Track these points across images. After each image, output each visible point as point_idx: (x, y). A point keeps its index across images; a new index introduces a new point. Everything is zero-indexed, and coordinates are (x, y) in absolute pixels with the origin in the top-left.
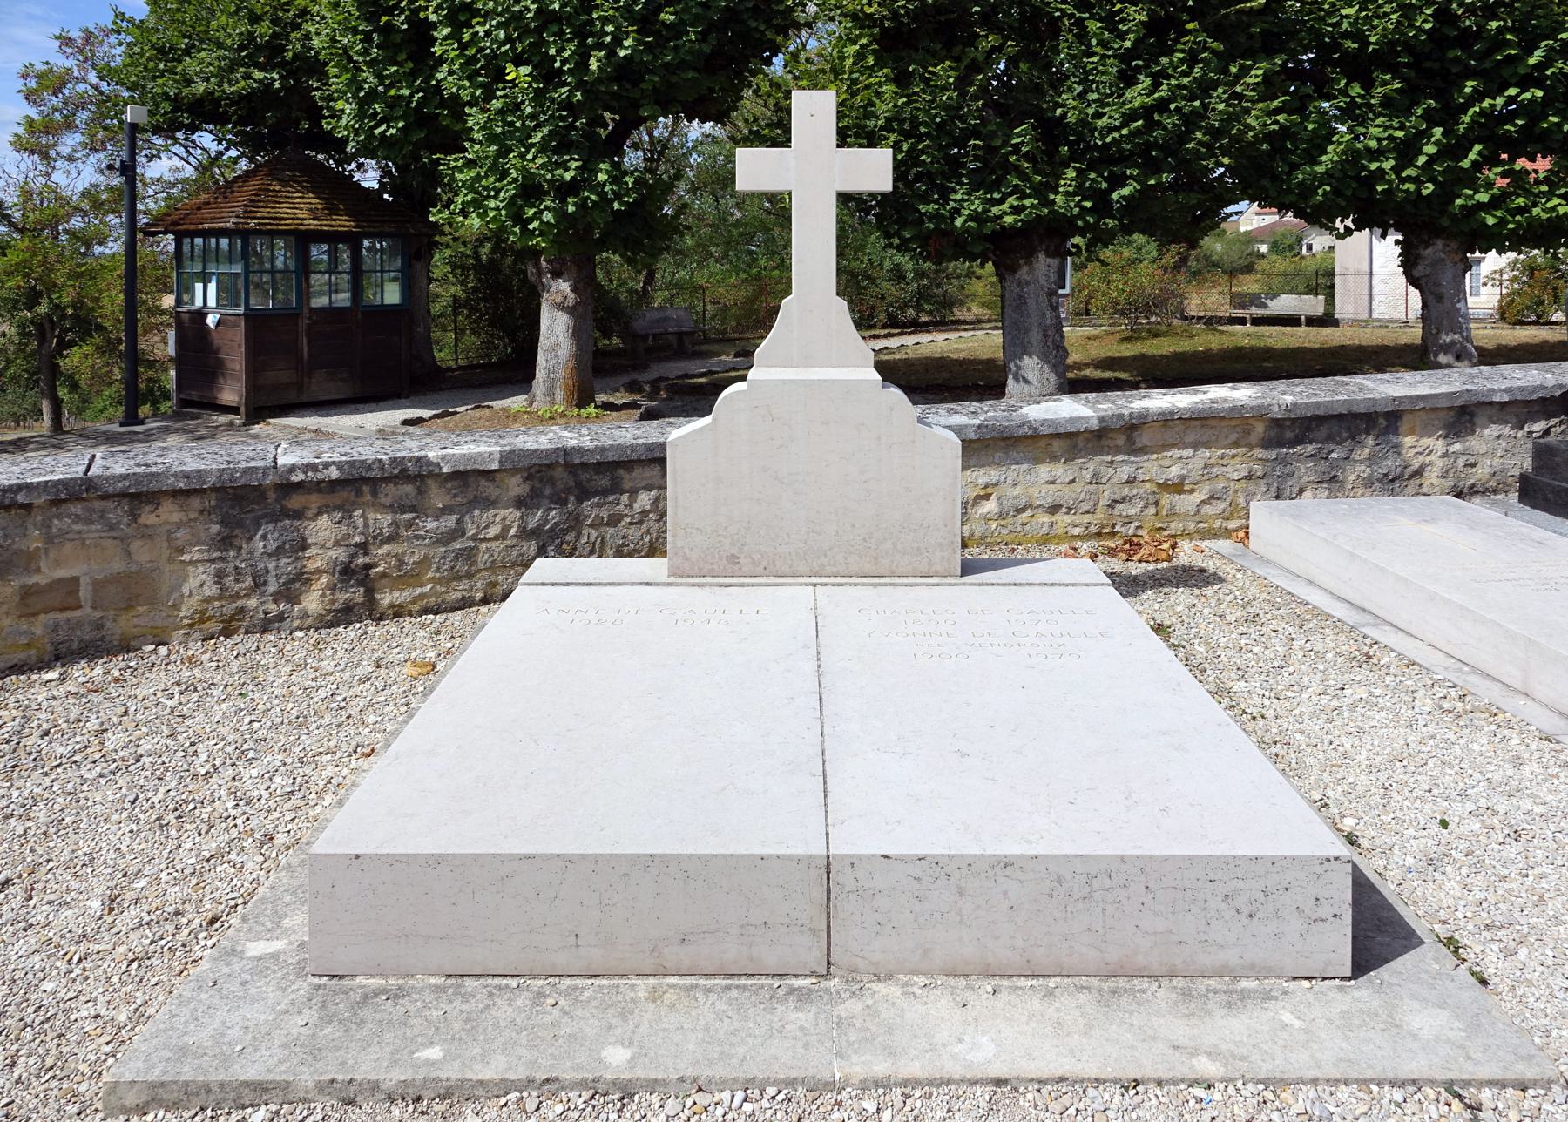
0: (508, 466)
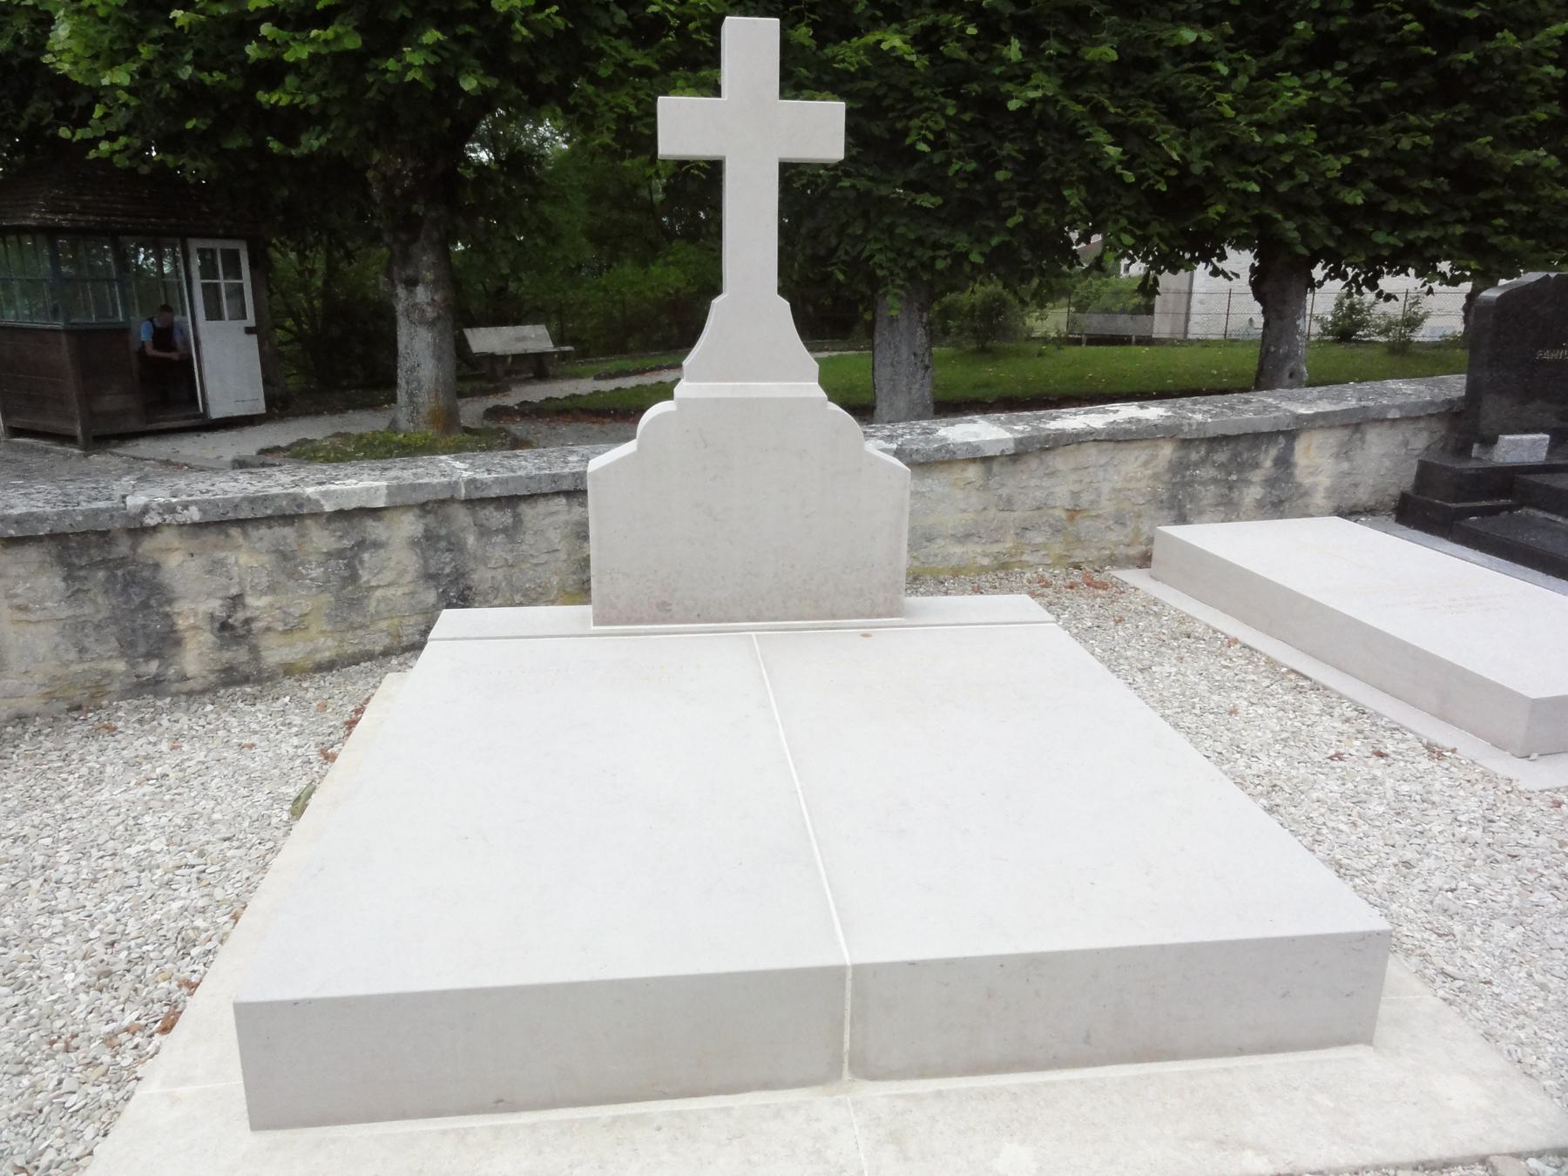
0: (399, 501)
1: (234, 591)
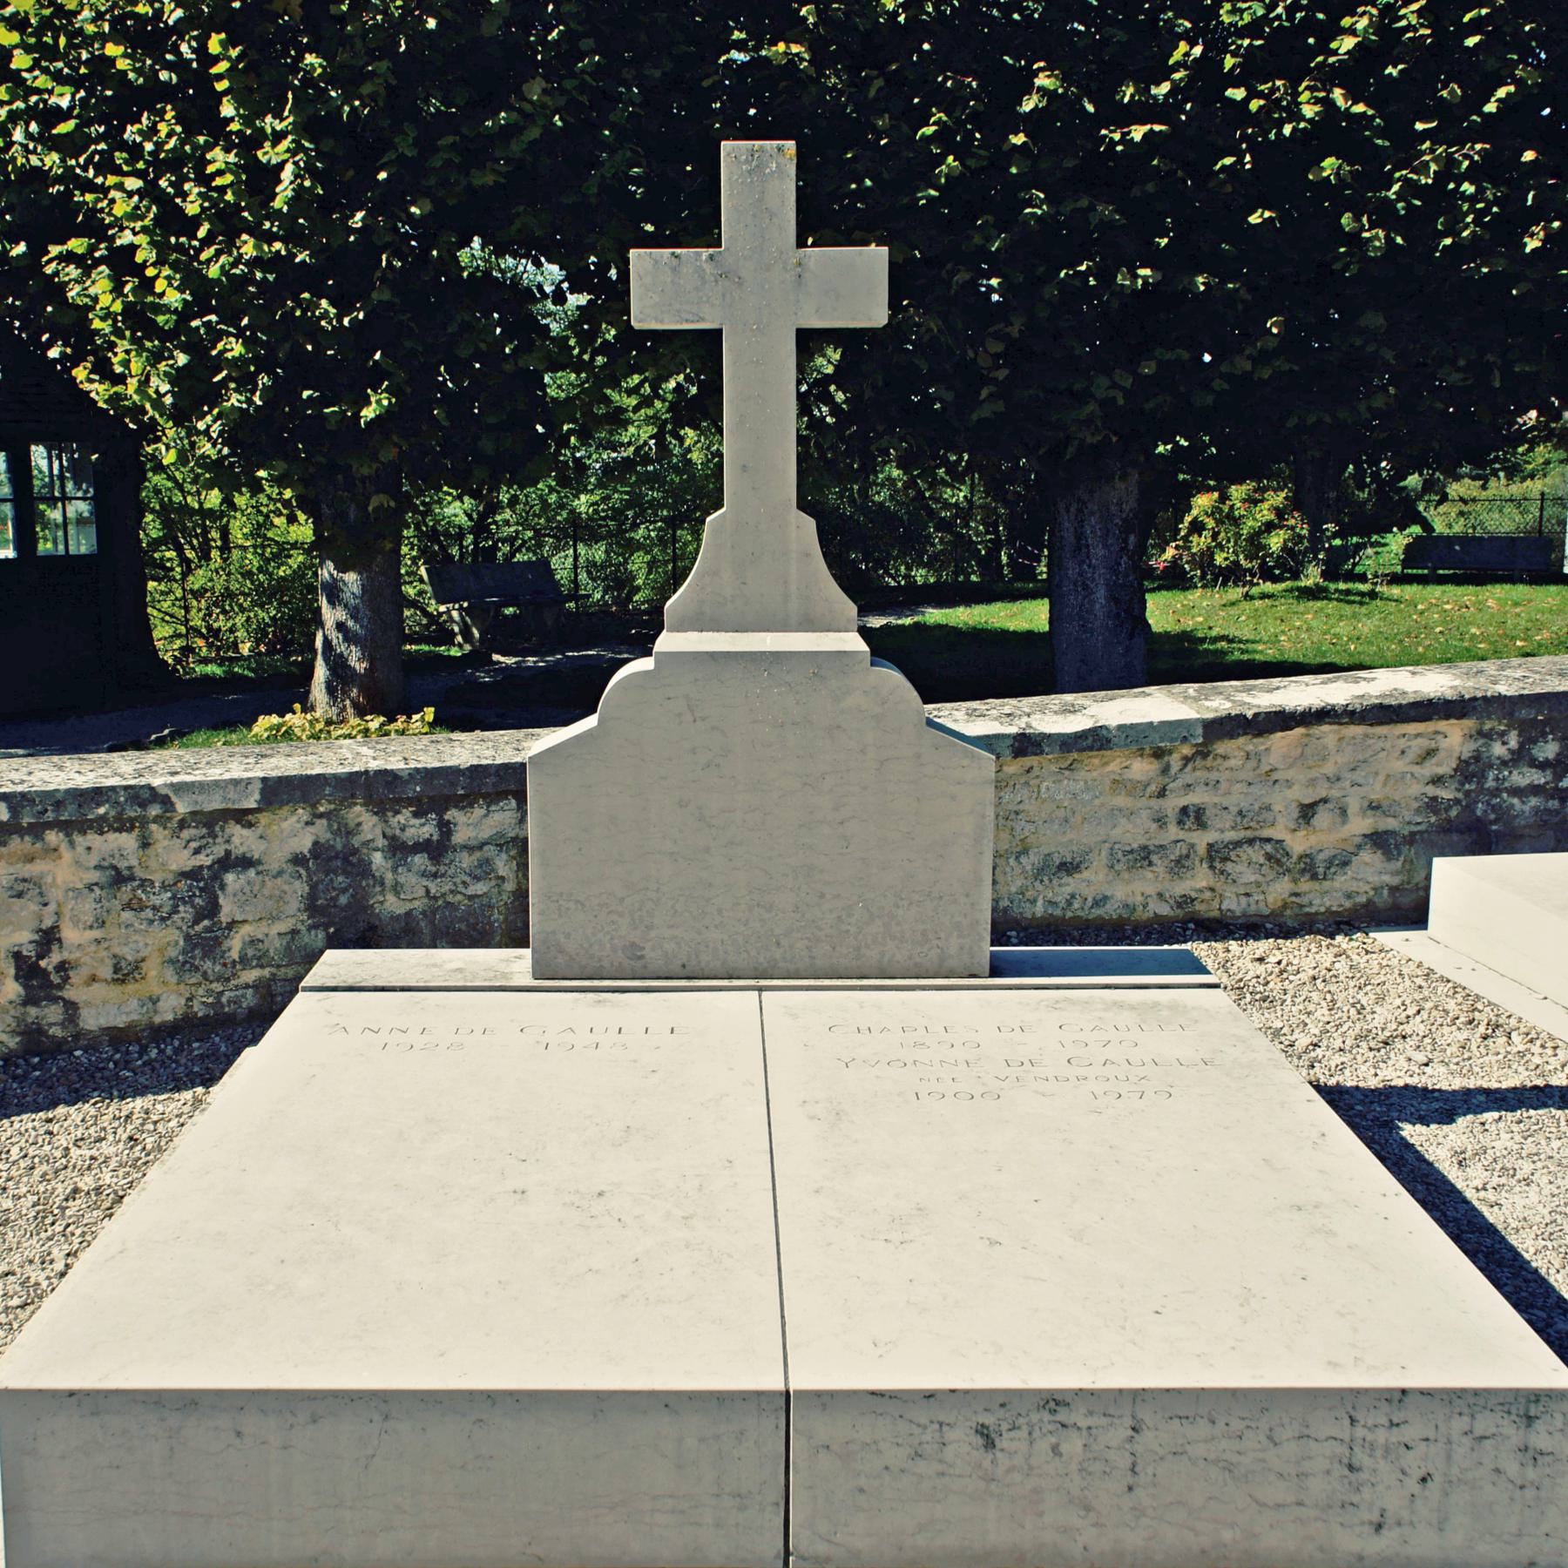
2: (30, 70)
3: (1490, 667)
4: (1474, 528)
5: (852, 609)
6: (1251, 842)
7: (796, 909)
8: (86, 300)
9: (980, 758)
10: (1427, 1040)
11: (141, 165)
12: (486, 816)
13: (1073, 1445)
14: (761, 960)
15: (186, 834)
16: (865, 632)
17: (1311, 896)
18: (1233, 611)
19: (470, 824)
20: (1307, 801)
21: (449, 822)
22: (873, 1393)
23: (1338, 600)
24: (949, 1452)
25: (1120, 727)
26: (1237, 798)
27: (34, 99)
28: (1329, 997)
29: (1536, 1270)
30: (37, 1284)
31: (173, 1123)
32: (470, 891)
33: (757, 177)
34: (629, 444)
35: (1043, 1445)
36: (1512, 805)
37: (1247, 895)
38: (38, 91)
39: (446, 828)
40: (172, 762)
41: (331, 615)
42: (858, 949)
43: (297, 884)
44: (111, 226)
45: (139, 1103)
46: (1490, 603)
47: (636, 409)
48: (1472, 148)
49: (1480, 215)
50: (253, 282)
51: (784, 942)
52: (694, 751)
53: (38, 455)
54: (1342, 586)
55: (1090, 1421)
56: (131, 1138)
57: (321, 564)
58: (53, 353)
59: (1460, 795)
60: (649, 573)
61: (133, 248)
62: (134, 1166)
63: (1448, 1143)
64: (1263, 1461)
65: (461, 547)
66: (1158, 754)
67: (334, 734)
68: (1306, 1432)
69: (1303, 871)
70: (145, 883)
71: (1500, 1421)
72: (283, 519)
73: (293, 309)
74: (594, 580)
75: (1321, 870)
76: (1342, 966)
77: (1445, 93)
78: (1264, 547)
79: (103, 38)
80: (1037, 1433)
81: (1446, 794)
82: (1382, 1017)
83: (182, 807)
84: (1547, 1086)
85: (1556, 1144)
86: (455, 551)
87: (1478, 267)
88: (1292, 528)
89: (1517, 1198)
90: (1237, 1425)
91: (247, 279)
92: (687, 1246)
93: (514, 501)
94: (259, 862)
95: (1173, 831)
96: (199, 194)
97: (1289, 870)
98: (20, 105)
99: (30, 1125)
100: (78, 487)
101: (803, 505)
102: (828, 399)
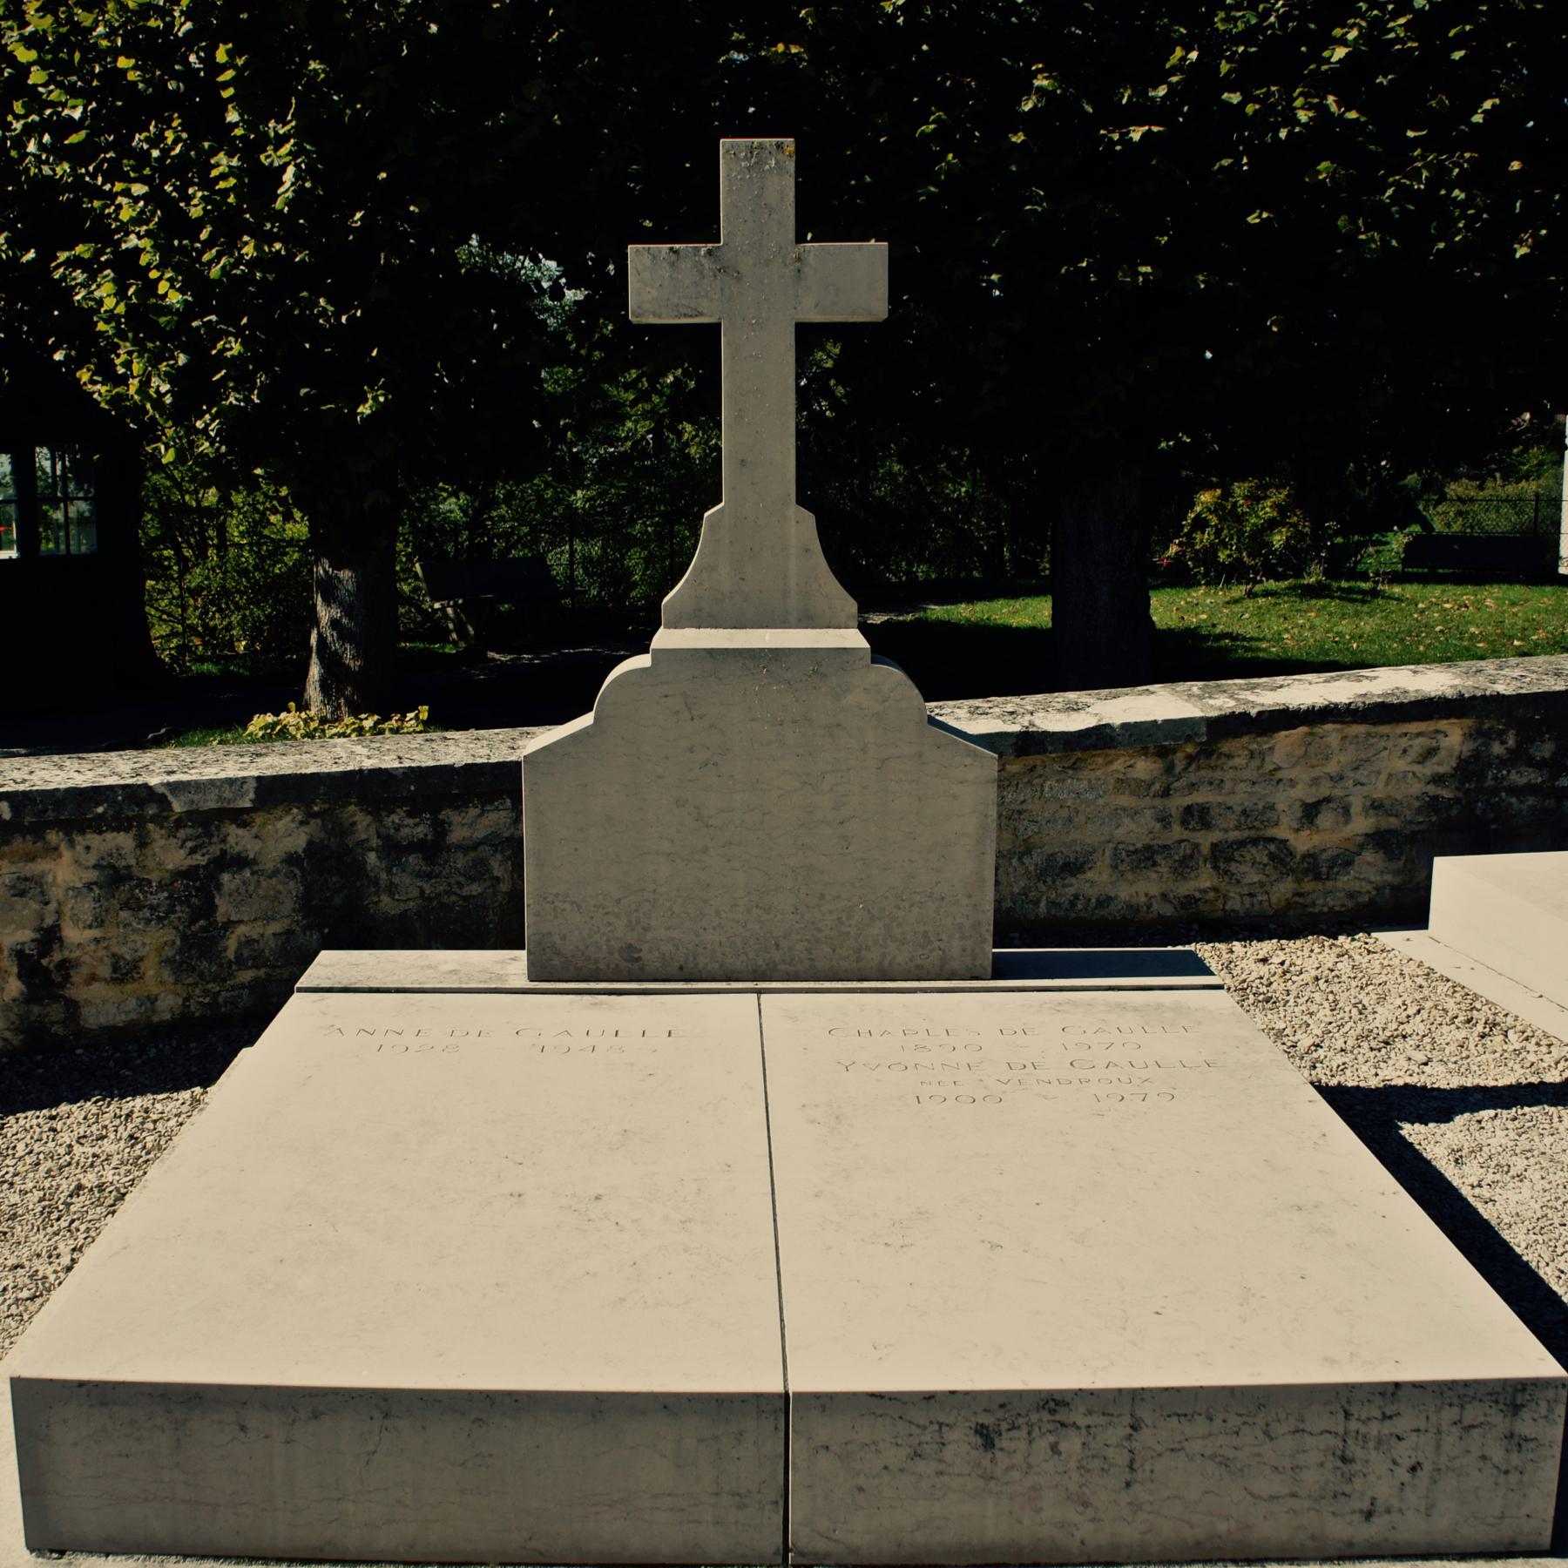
1: (49, 921)
2: (45, 85)
3: (1489, 666)
4: (1472, 527)
5: (852, 606)
6: (1255, 841)
7: (796, 911)
8: (91, 303)
9: (983, 757)
10: (1427, 1040)
11: (147, 171)
12: (480, 816)
13: (1072, 1444)
14: (760, 962)
15: (182, 834)
16: (865, 629)
17: (1314, 896)
18: (1236, 608)
19: (466, 825)
20: (1310, 800)
21: (443, 822)
22: (873, 1395)
23: (1340, 598)
24: (948, 1452)
25: (1125, 726)
26: (1240, 797)
27: (48, 112)
28: (1331, 997)
29: (1527, 1263)
30: (45, 1277)
31: (172, 1123)
32: (466, 891)
33: (755, 176)
34: (627, 438)
35: (1042, 1444)
36: (1511, 804)
37: (1251, 895)
38: (53, 104)
39: (441, 828)
40: (169, 761)
41: (325, 613)
42: (859, 950)
43: (292, 884)
44: (117, 231)
45: (139, 1102)
46: (1489, 602)
47: (634, 403)
48: (1462, 156)
49: (1470, 221)
50: (253, 281)
51: (784, 944)
52: (691, 750)
53: (43, 458)
54: (1344, 584)
55: (1089, 1420)
56: (131, 1137)
57: (317, 563)
58: (58, 356)
59: (1460, 795)
60: (646, 569)
61: (137, 251)
62: (135, 1164)
63: (1445, 1142)
64: (1259, 1455)
65: (456, 543)
66: (1163, 753)
67: (329, 733)
68: (1302, 1426)
69: (1306, 872)
70: (143, 883)
71: (1488, 1411)
72: (279, 517)
73: (292, 308)
74: (590, 575)
75: (1324, 870)
76: (1344, 967)
77: (1433, 103)
78: (1269, 545)
79: (115, 52)
80: (1036, 1433)
81: (1446, 793)
82: (1383, 1017)
83: (178, 807)
84: (1542, 1083)
85: (1548, 1140)
86: (450, 548)
87: (1471, 271)
88: (1295, 526)
89: (1510, 1194)
90: (1234, 1421)
91: (247, 279)
92: (685, 1250)
93: (509, 497)
94: (255, 861)
95: (1177, 831)
96: (203, 198)
97: (1292, 870)
98: (35, 117)
99: (35, 1122)
100: (79, 487)
101: (802, 500)
102: (829, 394)
